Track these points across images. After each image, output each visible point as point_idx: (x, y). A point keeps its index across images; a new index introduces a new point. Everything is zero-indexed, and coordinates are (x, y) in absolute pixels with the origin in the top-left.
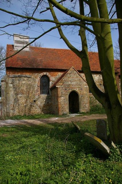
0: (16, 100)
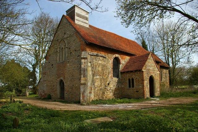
0: (93, 82)
